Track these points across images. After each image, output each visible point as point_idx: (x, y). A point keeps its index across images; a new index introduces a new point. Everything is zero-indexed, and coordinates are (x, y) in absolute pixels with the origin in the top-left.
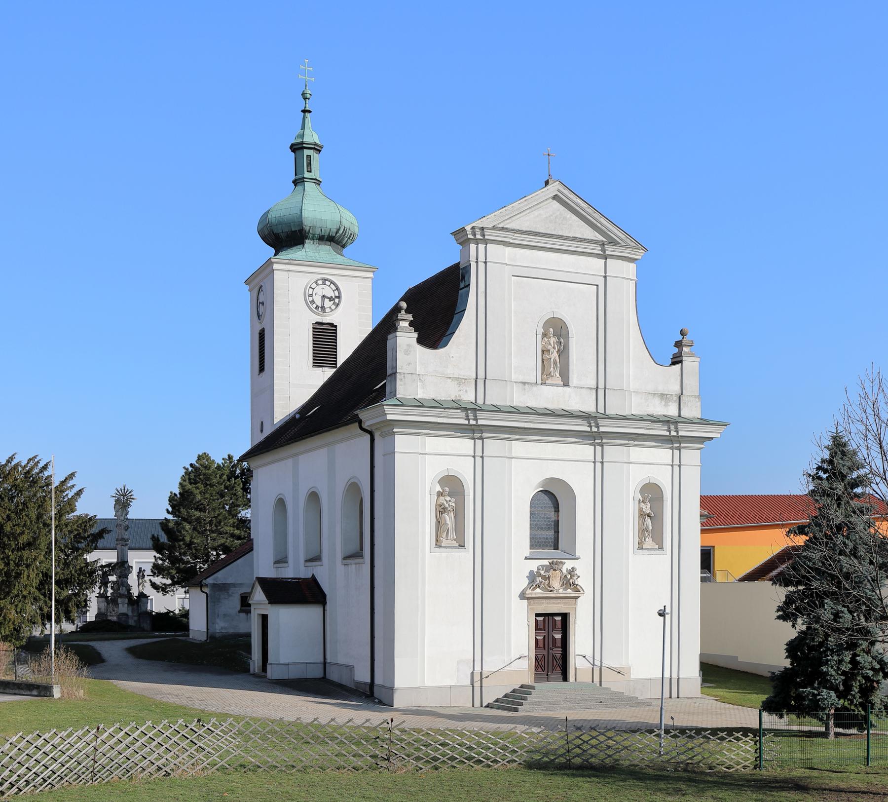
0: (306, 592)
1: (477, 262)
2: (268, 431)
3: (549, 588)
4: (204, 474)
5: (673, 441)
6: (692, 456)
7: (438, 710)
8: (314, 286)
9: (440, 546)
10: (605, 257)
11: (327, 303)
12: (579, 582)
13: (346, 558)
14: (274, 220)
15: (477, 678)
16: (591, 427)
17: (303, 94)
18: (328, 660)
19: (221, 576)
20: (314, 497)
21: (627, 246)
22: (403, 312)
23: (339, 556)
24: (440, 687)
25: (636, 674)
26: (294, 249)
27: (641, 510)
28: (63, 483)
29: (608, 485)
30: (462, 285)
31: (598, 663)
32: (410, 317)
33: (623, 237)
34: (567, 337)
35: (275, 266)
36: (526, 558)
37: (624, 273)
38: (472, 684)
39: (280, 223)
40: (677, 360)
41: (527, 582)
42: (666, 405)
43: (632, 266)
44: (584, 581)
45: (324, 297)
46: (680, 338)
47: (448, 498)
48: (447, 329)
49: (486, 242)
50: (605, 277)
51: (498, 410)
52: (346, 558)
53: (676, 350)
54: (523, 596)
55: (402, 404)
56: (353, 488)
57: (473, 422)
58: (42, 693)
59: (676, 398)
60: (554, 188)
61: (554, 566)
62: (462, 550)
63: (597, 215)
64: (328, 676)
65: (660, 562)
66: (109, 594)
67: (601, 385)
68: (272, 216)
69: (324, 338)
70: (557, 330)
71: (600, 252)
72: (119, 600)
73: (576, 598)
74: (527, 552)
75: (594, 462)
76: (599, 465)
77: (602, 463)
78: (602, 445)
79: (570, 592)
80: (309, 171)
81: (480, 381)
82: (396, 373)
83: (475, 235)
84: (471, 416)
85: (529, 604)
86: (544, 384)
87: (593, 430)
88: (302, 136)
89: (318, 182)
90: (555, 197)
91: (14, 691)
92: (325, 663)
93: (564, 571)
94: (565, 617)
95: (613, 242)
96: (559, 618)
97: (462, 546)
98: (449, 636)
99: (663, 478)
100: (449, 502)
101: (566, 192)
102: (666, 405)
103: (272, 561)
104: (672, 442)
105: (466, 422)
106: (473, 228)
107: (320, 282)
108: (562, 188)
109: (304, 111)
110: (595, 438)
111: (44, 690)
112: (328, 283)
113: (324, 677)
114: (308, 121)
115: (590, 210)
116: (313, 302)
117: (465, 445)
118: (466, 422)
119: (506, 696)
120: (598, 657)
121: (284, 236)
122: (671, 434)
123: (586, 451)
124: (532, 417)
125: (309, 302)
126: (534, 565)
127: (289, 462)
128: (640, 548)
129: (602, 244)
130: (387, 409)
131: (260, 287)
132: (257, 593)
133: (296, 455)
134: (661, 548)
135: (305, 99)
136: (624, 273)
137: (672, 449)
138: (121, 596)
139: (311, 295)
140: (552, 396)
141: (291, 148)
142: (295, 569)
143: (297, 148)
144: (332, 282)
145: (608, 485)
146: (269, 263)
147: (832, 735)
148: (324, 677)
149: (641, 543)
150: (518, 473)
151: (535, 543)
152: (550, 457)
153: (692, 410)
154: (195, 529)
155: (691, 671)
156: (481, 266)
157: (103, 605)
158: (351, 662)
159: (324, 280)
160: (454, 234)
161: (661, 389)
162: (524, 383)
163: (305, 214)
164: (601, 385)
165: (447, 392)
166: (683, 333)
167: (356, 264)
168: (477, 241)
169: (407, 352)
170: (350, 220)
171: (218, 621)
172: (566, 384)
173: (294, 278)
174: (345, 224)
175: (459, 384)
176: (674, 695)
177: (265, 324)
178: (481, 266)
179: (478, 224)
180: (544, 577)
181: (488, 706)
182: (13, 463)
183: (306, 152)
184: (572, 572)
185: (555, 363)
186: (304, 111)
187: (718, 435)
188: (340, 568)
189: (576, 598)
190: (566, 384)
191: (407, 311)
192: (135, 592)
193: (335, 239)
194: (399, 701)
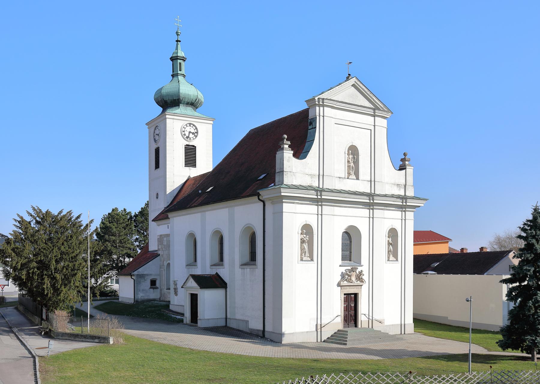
1: (319, 116)
3: (350, 281)
4: (117, 218)
5: (402, 208)
6: (410, 215)
7: (304, 345)
8: (185, 127)
10: (374, 116)
11: (191, 136)
12: (363, 277)
13: (242, 265)
14: (165, 93)
15: (319, 327)
16: (370, 200)
17: (177, 33)
18: (228, 316)
19: (141, 271)
21: (384, 111)
22: (285, 140)
23: (237, 263)
24: (302, 333)
25: (387, 323)
26: (174, 108)
27: (388, 241)
28: (87, 225)
30: (310, 127)
31: (371, 318)
32: (289, 143)
33: (382, 106)
35: (167, 116)
36: (340, 266)
37: (382, 123)
38: (317, 330)
39: (168, 95)
40: (402, 168)
41: (340, 277)
42: (399, 190)
44: (365, 277)
45: (190, 132)
46: (403, 157)
47: (305, 236)
49: (323, 106)
50: (374, 126)
51: (331, 191)
52: (242, 265)
54: (339, 285)
55: (289, 187)
57: (319, 197)
58: (102, 341)
59: (403, 186)
60: (352, 81)
61: (353, 270)
62: (312, 262)
63: (371, 95)
64: (228, 325)
65: (396, 267)
67: (373, 180)
68: (164, 91)
70: (353, 151)
73: (361, 285)
74: (340, 262)
75: (369, 218)
76: (371, 219)
77: (321, 215)
78: (373, 209)
79: (359, 283)
80: (180, 70)
81: (321, 176)
83: (319, 102)
84: (319, 194)
85: (341, 289)
86: (348, 178)
87: (371, 201)
89: (184, 76)
91: (81, 340)
92: (226, 318)
93: (357, 272)
94: (356, 295)
95: (379, 109)
96: (353, 296)
97: (312, 260)
98: (306, 308)
99: (398, 226)
101: (359, 83)
102: (399, 190)
103: (184, 264)
104: (402, 208)
105: (316, 197)
106: (319, 99)
107: (188, 125)
108: (357, 81)
109: (177, 41)
110: (370, 206)
111: (103, 340)
113: (226, 326)
114: (179, 46)
115: (369, 93)
116: (185, 135)
117: (313, 208)
118: (316, 197)
119: (332, 336)
120: (371, 315)
121: (169, 102)
122: (402, 204)
123: (365, 212)
124: (346, 195)
125: (183, 135)
126: (343, 269)
127: (199, 214)
128: (388, 260)
130: (282, 190)
134: (397, 260)
135: (178, 35)
136: (382, 123)
137: (402, 211)
139: (184, 131)
140: (351, 185)
141: (170, 59)
143: (174, 59)
144: (194, 125)
147: (536, 360)
148: (226, 326)
149: (389, 258)
150: (336, 221)
151: (343, 259)
153: (410, 193)
154: (112, 246)
155: (409, 320)
156: (321, 118)
158: (247, 319)
159: (190, 124)
161: (397, 182)
162: (340, 178)
163: (181, 91)
164: (373, 180)
165: (306, 181)
167: (205, 116)
168: (319, 106)
169: (288, 161)
170: (201, 96)
171: (139, 293)
172: (358, 179)
173: (175, 124)
174: (199, 97)
175: (312, 178)
176: (403, 333)
177: (160, 145)
178: (321, 118)
179: (321, 96)
180: (349, 276)
181: (324, 342)
182: (62, 215)
183: (179, 61)
185: (353, 167)
186: (177, 41)
187: (423, 205)
188: (238, 270)
189: (361, 285)
190: (358, 179)
191: (287, 140)
193: (193, 104)
194: (285, 341)
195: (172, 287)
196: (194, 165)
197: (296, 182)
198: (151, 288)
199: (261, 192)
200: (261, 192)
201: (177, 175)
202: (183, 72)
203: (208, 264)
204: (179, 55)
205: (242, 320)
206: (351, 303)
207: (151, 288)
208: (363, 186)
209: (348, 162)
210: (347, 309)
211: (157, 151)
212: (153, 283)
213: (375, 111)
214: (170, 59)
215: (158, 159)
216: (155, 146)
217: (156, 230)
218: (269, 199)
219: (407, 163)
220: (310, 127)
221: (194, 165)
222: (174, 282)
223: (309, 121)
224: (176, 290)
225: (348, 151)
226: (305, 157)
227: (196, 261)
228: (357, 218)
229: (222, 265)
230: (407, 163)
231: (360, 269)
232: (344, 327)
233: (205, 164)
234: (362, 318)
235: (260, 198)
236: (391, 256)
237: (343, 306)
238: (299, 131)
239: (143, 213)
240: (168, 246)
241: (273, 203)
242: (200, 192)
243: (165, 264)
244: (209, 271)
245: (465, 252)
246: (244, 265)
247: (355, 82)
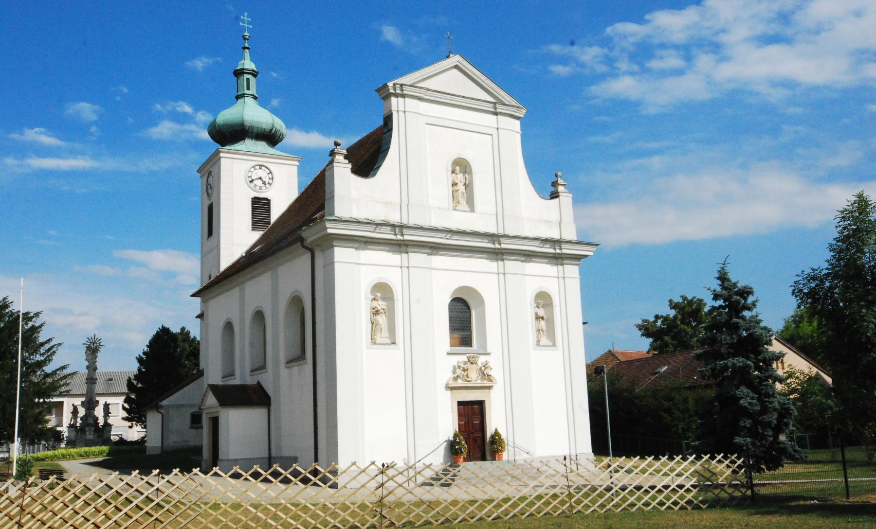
0: (254, 396)
2: (215, 274)
3: (467, 378)
9: (375, 343)
10: (496, 114)
13: (288, 362)
18: (273, 455)
20: (259, 316)
27: (536, 314)
29: (506, 293)
35: (222, 155)
40: (554, 195)
43: (518, 123)
44: (495, 372)
48: (375, 164)
49: (404, 96)
56: (296, 301)
57: (400, 240)
66: (78, 425)
67: (500, 213)
69: (260, 206)
70: (461, 166)
71: (493, 110)
72: (87, 429)
73: (489, 388)
74: (448, 348)
83: (395, 90)
87: (495, 248)
97: (394, 343)
99: (552, 288)
100: (381, 305)
106: (394, 84)
126: (456, 360)
127: (237, 289)
128: (538, 345)
129: (495, 104)
130: (328, 225)
131: (209, 172)
132: (209, 398)
133: (243, 283)
134: (554, 345)
138: (88, 425)
142: (242, 377)
145: (506, 293)
146: (217, 153)
150: (437, 280)
152: (462, 269)
153: (570, 234)
157: (73, 434)
159: (261, 166)
162: (439, 208)
164: (500, 213)
168: (396, 95)
170: (279, 124)
174: (276, 125)
180: (464, 370)
183: (246, 76)
184: (486, 366)
190: (472, 210)
192: (101, 422)
197: (357, 214)
207: (191, 428)
208: (481, 221)
211: (210, 209)
216: (207, 203)
246: (290, 362)
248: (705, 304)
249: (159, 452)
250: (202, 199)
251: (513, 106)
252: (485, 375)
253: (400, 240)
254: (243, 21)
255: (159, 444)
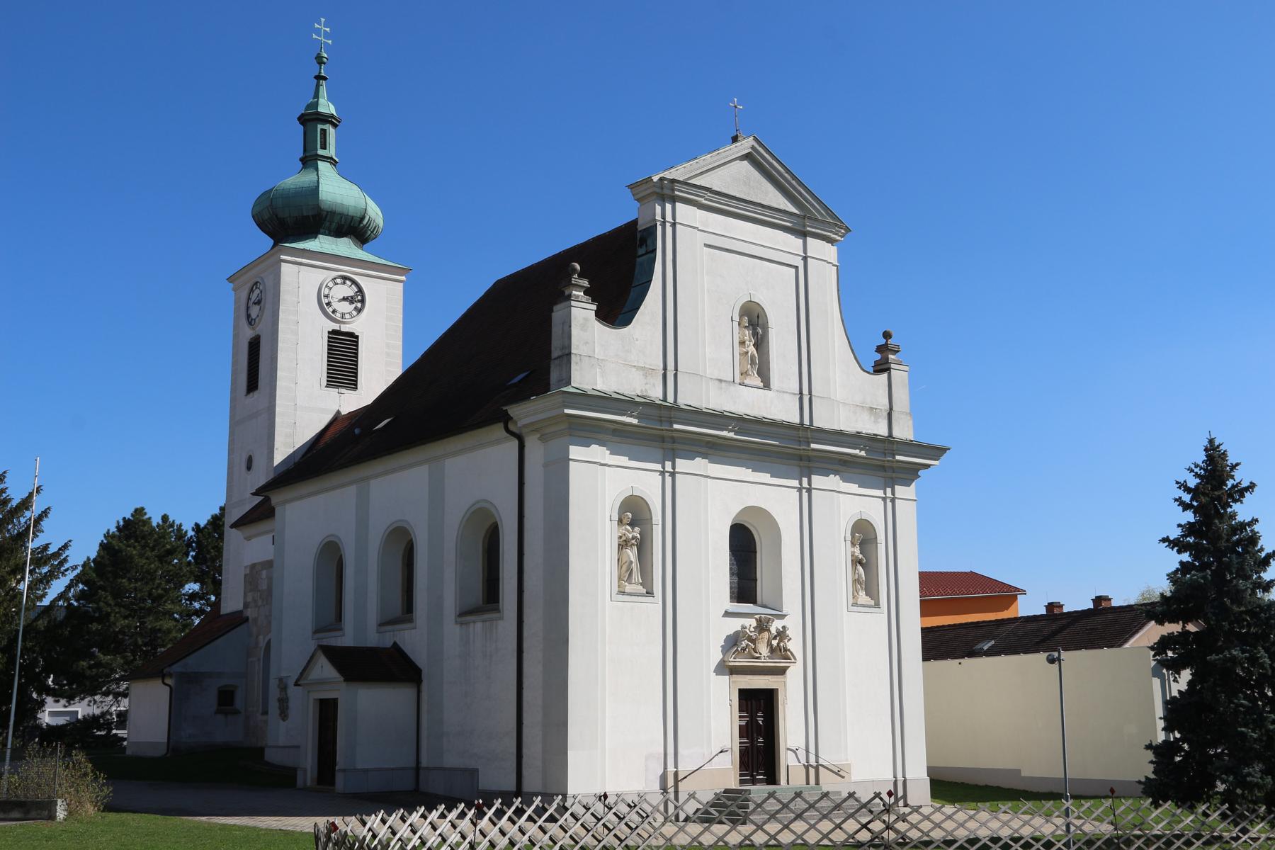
8: (331, 284)
10: (803, 234)
11: (346, 307)
12: (790, 646)
13: (462, 614)
15: (671, 782)
18: (424, 762)
19: (193, 662)
23: (450, 605)
30: (641, 251)
32: (586, 283)
34: (765, 328)
40: (881, 367)
42: (876, 422)
44: (794, 645)
46: (883, 341)
49: (674, 200)
50: (805, 259)
52: (462, 614)
53: (878, 356)
57: (662, 431)
61: (762, 626)
65: (876, 622)
67: (805, 391)
80: (324, 147)
81: (669, 373)
82: (570, 354)
87: (794, 450)
88: (316, 105)
90: (747, 157)
93: (773, 631)
97: (650, 593)
98: (633, 704)
102: (876, 422)
112: (348, 283)
125: (324, 306)
126: (735, 625)
127: (352, 489)
128: (855, 605)
133: (366, 479)
134: (877, 605)
141: (299, 119)
144: (354, 282)
148: (417, 790)
150: (714, 496)
153: (903, 431)
155: (918, 774)
159: (345, 278)
160: (631, 187)
162: (721, 381)
164: (805, 391)
166: (887, 335)
169: (584, 327)
170: (375, 213)
173: (305, 288)
174: (369, 209)
177: (262, 329)
188: (451, 629)
190: (767, 386)
191: (581, 276)
195: (274, 693)
196: (352, 384)
198: (218, 712)
199: (514, 410)
200: (514, 410)
201: (305, 406)
202: (331, 151)
203: (372, 618)
204: (321, 109)
205: (461, 770)
206: (759, 711)
207: (218, 712)
209: (742, 343)
210: (746, 732)
211: (254, 346)
212: (226, 698)
213: (807, 220)
214: (299, 119)
215: (255, 367)
216: (248, 333)
217: (242, 551)
218: (535, 428)
219: (891, 357)
220: (641, 251)
221: (352, 384)
222: (281, 680)
223: (639, 236)
224: (283, 703)
225: (741, 316)
226: (626, 322)
227: (340, 620)
228: (774, 496)
229: (411, 620)
230: (891, 357)
231: (776, 625)
232: (742, 782)
233: (380, 370)
234: (789, 760)
235: (511, 427)
236: (862, 593)
237: (737, 723)
238: (618, 270)
239: (216, 522)
240: (268, 595)
241: (544, 438)
242: (357, 431)
243: (262, 644)
244: (374, 639)
245: (1056, 611)
246: (466, 613)
247: (753, 148)
248: (1181, 563)
249: (161, 751)
250: (236, 327)
251: (823, 222)
252: (781, 652)
253: (662, 431)
254: (318, 32)
255: (163, 738)
